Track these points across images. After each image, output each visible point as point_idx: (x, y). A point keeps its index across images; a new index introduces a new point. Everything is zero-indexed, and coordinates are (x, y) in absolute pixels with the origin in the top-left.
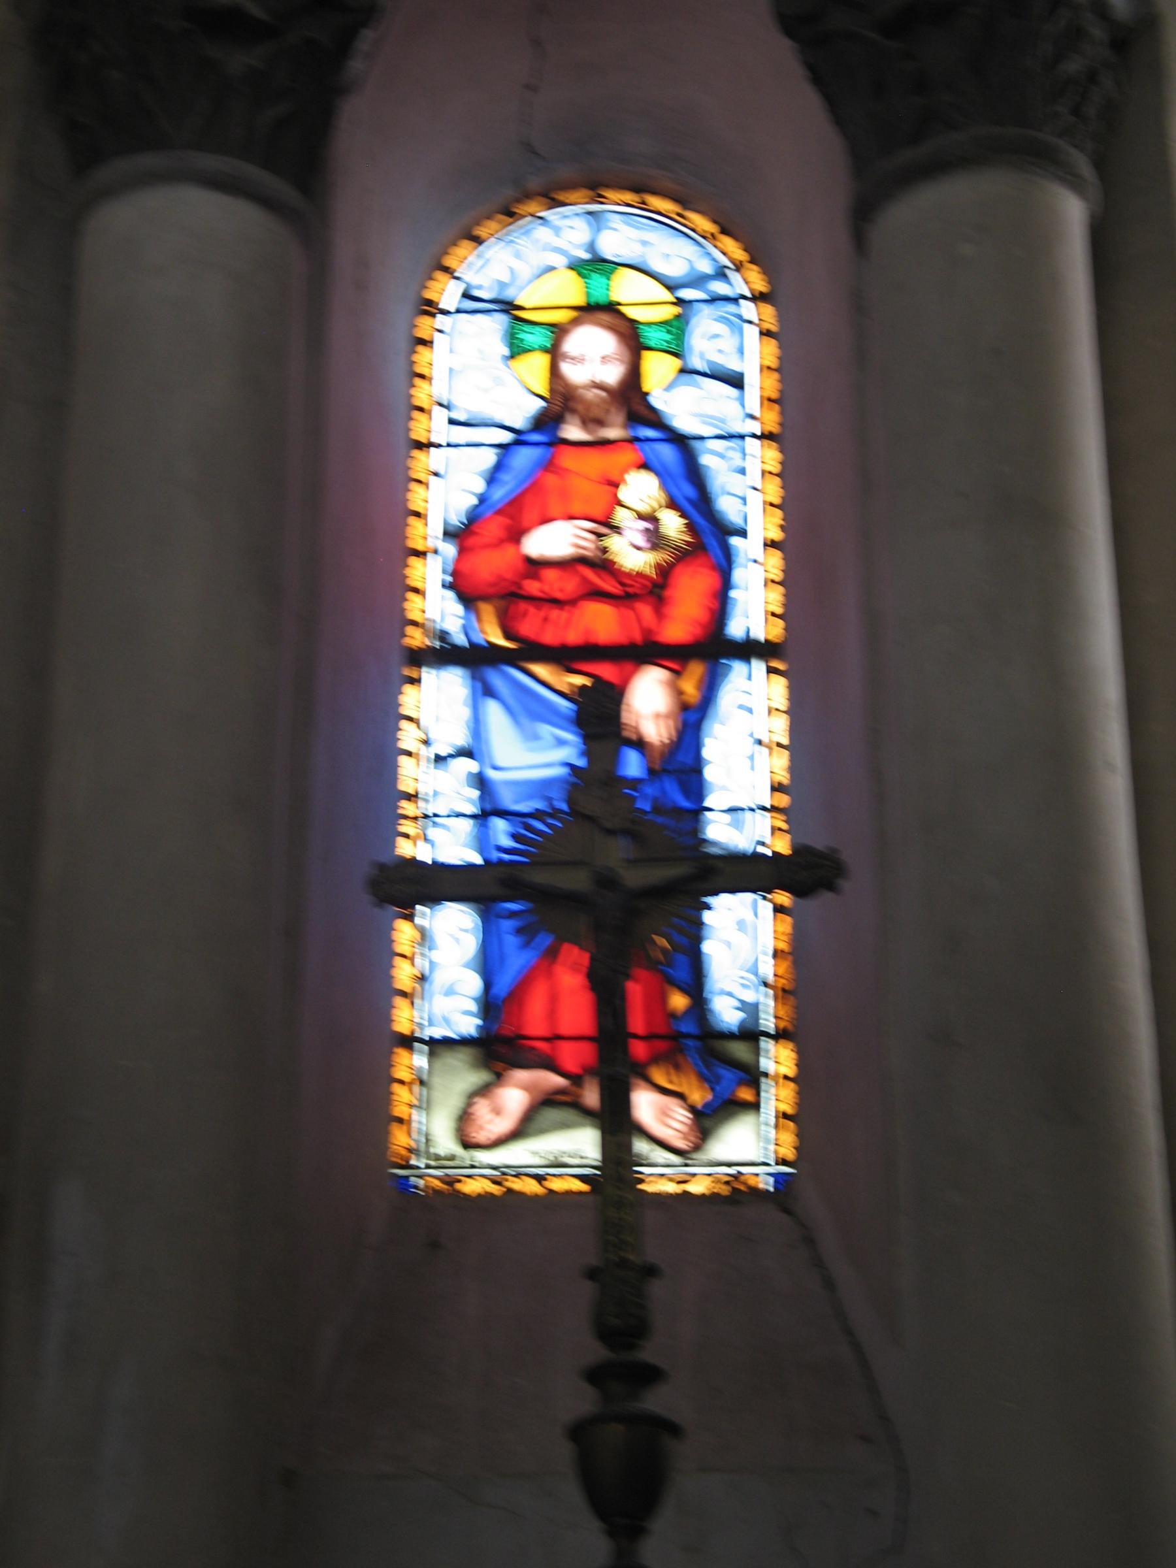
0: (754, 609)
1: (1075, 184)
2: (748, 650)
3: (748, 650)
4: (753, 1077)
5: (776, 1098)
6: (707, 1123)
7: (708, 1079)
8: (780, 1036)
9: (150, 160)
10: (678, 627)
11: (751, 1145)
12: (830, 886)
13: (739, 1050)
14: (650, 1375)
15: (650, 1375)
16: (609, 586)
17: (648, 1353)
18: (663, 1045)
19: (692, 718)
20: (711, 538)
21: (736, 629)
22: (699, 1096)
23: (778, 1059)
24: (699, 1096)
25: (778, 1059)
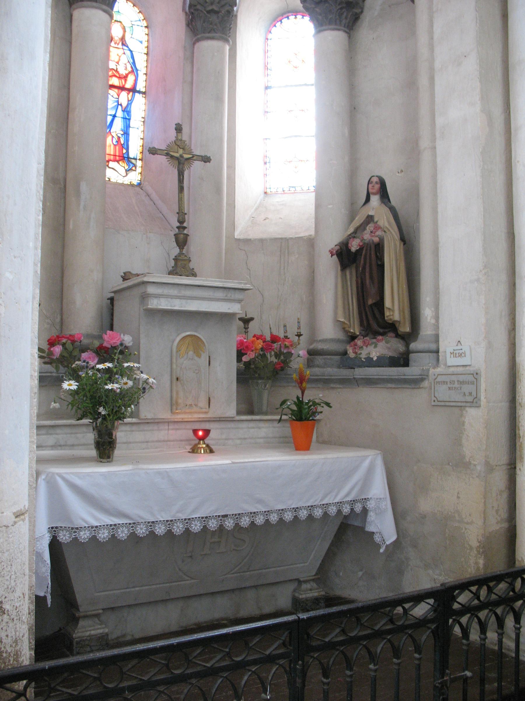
0: (141, 86)
1: (229, 45)
2: (139, 92)
3: (139, 92)
4: (135, 166)
5: (139, 170)
6: (128, 172)
7: (129, 166)
8: (140, 160)
9: (94, 4)
10: (129, 85)
11: (134, 177)
12: (209, 162)
13: (133, 161)
14: (185, 228)
15: (185, 228)
16: (118, 75)
17: (185, 225)
18: (121, 158)
19: (130, 102)
20: (134, 70)
21: (138, 89)
22: (127, 167)
23: (139, 163)
24: (127, 167)
25: (139, 163)
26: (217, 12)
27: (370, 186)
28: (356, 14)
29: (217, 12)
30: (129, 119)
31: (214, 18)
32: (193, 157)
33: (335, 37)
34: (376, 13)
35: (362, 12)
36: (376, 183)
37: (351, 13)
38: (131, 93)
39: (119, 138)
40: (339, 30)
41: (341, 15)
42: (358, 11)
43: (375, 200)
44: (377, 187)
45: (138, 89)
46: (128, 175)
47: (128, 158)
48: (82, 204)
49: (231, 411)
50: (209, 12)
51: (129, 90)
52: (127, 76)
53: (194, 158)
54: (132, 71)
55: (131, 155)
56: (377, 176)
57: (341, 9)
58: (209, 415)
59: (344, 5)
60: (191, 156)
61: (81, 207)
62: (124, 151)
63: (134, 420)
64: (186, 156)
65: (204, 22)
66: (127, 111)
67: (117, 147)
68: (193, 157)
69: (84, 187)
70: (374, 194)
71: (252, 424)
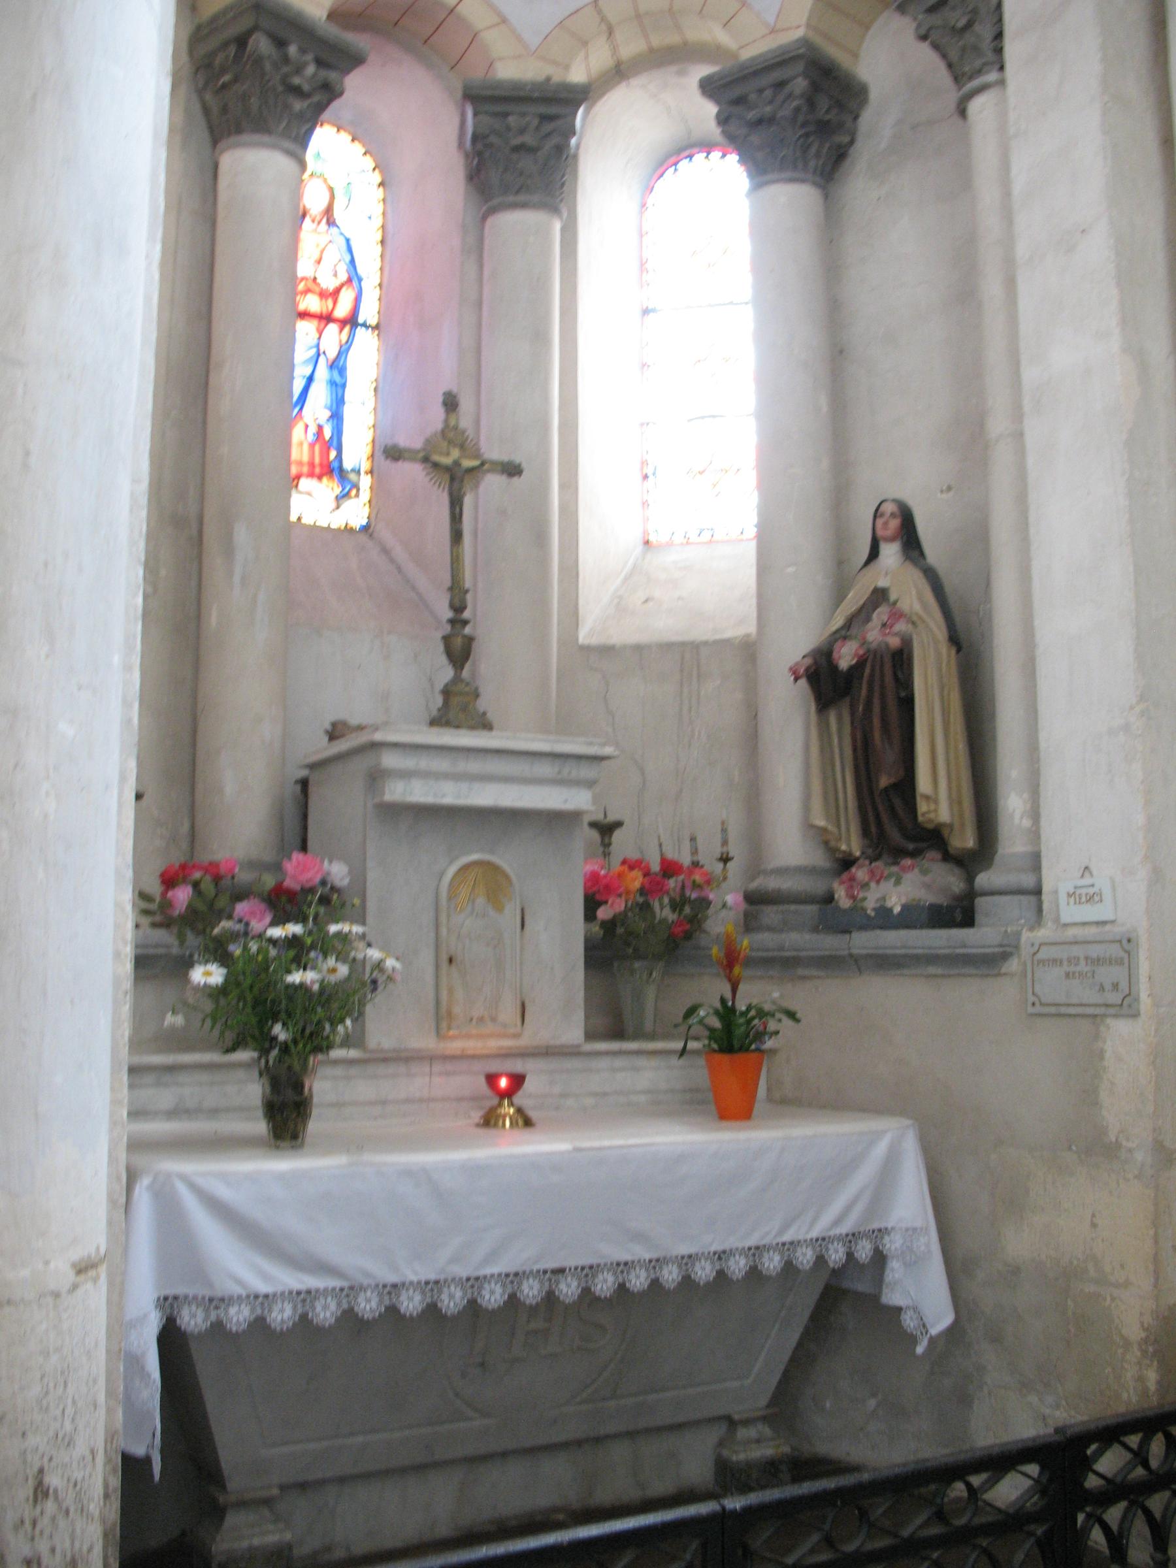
0: (369, 312)
2: (364, 325)
4: (356, 486)
20: (353, 279)
26: (533, 150)
27: (879, 522)
28: (840, 146)
29: (533, 150)
30: (344, 386)
31: (526, 163)
32: (483, 464)
33: (795, 197)
34: (883, 146)
35: (852, 142)
36: (893, 515)
37: (827, 145)
38: (347, 329)
39: (320, 428)
40: (803, 181)
41: (805, 149)
42: (846, 139)
43: (891, 553)
44: (895, 524)
45: (361, 320)
46: (342, 507)
47: (341, 469)
48: (238, 571)
49: (573, 1032)
50: (517, 149)
51: (343, 323)
52: (337, 291)
53: (486, 467)
54: (349, 281)
55: (348, 465)
56: (894, 501)
57: (807, 135)
58: (524, 1041)
59: (811, 128)
60: (476, 463)
61: (237, 578)
62: (333, 454)
63: (353, 1053)
64: (467, 463)
65: (505, 170)
66: (338, 366)
67: (317, 448)
68: (483, 464)
69: (241, 535)
70: (892, 539)
71: (619, 1062)
